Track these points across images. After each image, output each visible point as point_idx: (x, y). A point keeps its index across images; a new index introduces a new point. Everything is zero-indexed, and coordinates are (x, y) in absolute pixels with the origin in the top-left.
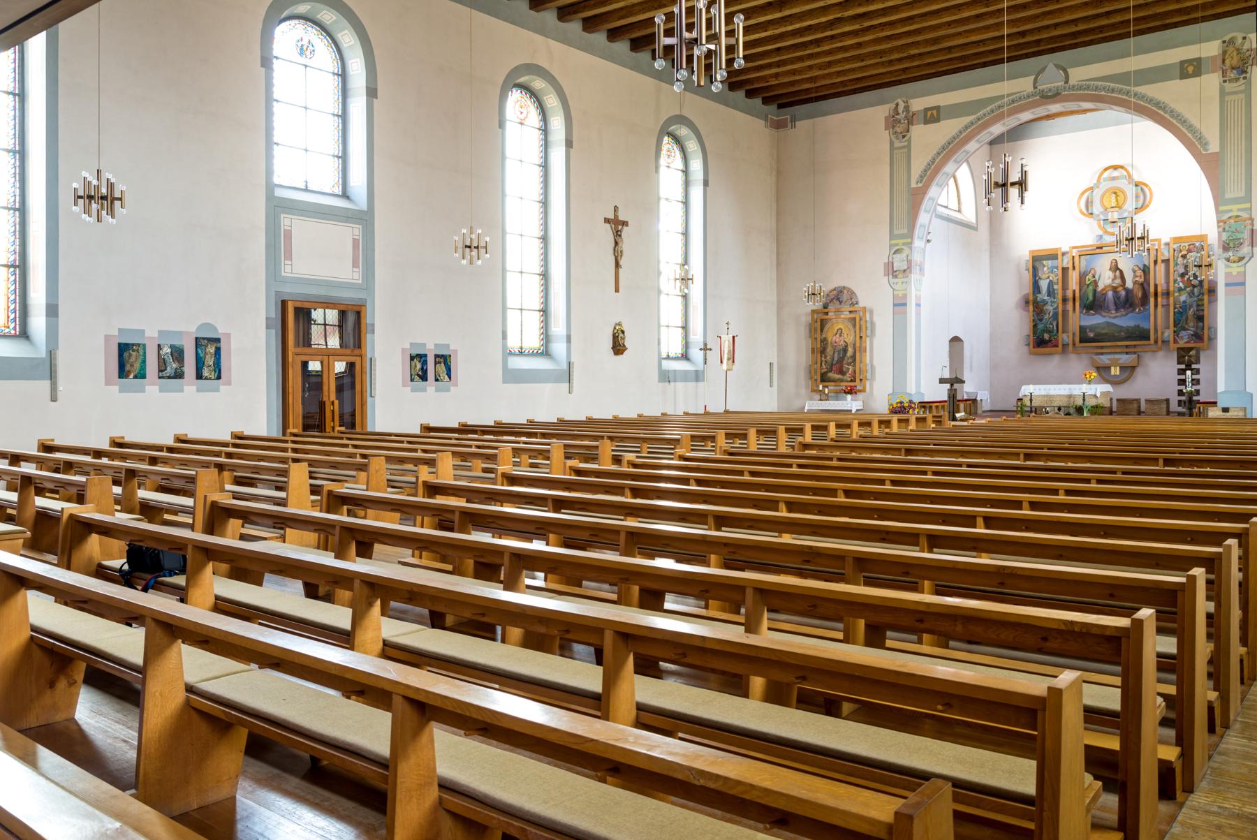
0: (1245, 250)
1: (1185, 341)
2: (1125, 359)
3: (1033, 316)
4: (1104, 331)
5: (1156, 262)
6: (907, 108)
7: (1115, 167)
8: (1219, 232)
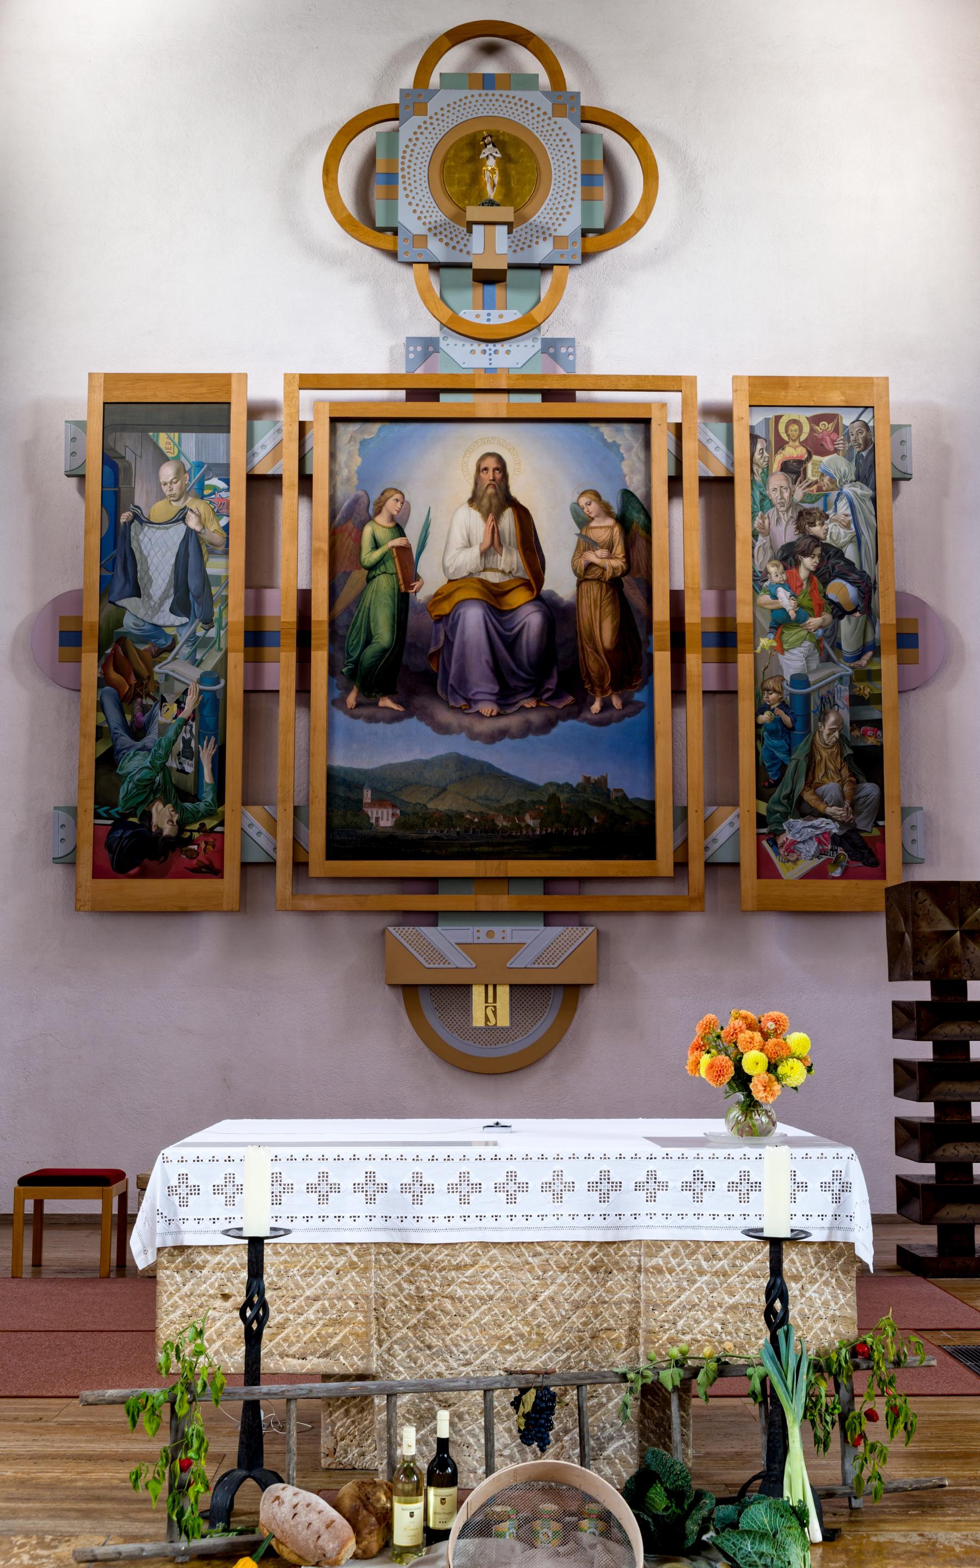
1: (807, 865)
3: (101, 707)
5: (675, 483)
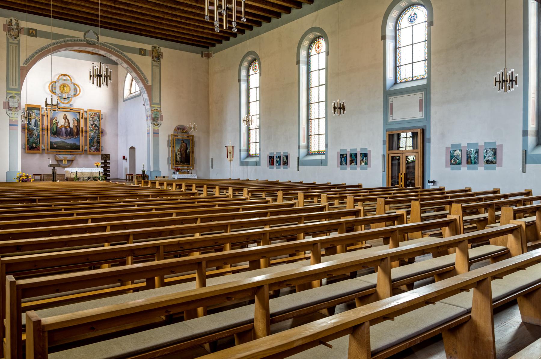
0: (159, 122)
1: (93, 151)
2: (69, 157)
3: (27, 135)
4: (60, 145)
6: (17, 24)
7: (64, 75)
8: (151, 114)
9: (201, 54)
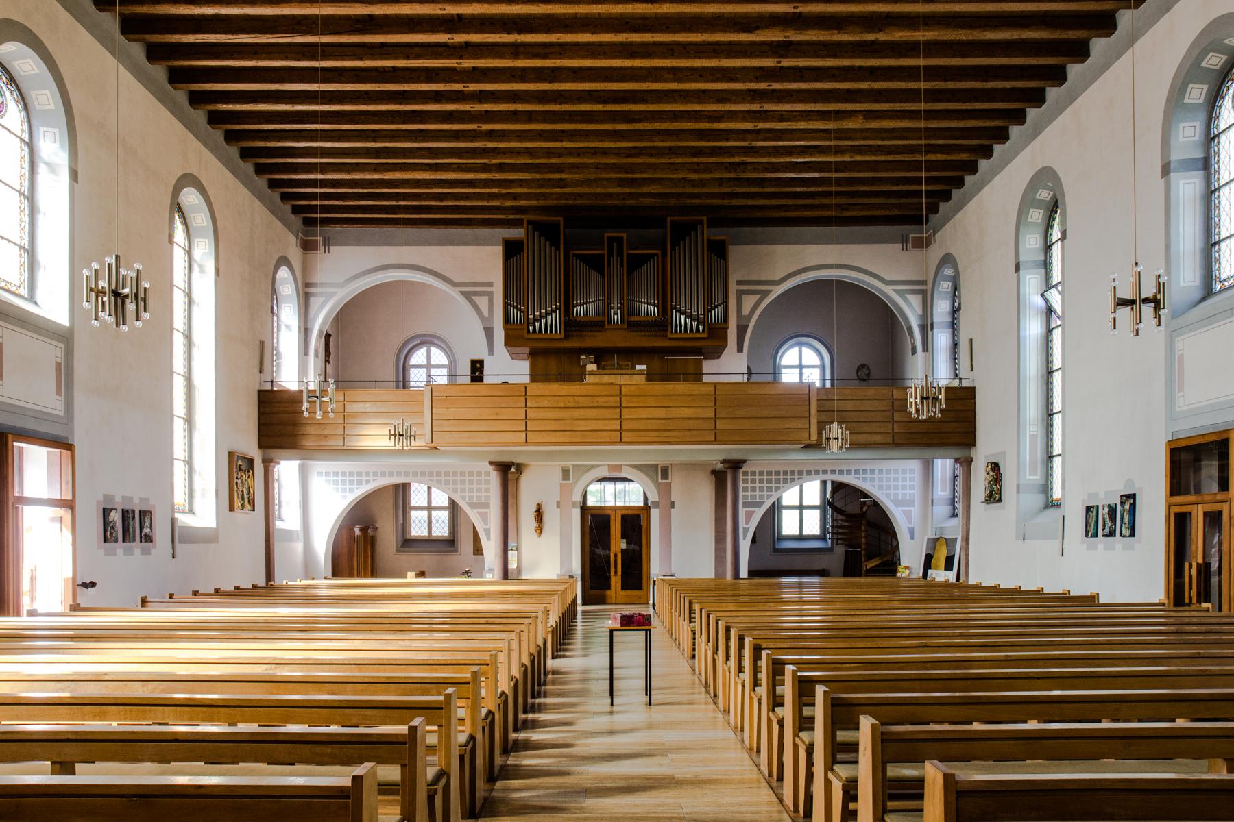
9: (902, 243)
